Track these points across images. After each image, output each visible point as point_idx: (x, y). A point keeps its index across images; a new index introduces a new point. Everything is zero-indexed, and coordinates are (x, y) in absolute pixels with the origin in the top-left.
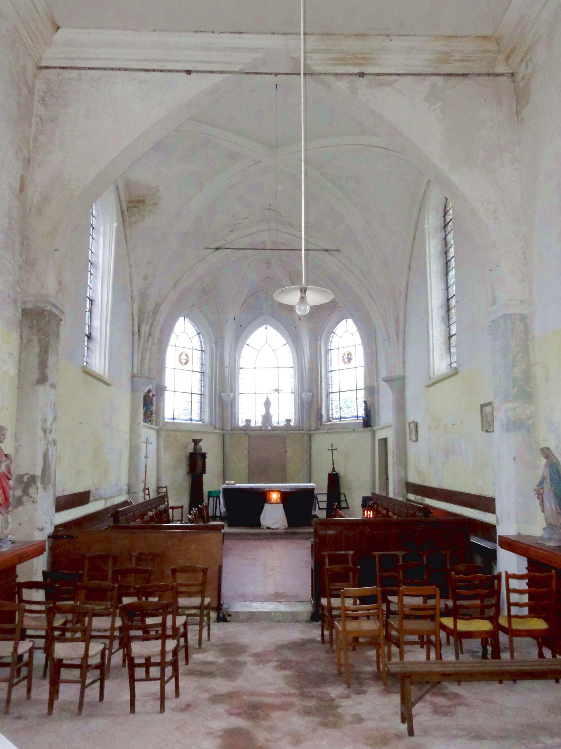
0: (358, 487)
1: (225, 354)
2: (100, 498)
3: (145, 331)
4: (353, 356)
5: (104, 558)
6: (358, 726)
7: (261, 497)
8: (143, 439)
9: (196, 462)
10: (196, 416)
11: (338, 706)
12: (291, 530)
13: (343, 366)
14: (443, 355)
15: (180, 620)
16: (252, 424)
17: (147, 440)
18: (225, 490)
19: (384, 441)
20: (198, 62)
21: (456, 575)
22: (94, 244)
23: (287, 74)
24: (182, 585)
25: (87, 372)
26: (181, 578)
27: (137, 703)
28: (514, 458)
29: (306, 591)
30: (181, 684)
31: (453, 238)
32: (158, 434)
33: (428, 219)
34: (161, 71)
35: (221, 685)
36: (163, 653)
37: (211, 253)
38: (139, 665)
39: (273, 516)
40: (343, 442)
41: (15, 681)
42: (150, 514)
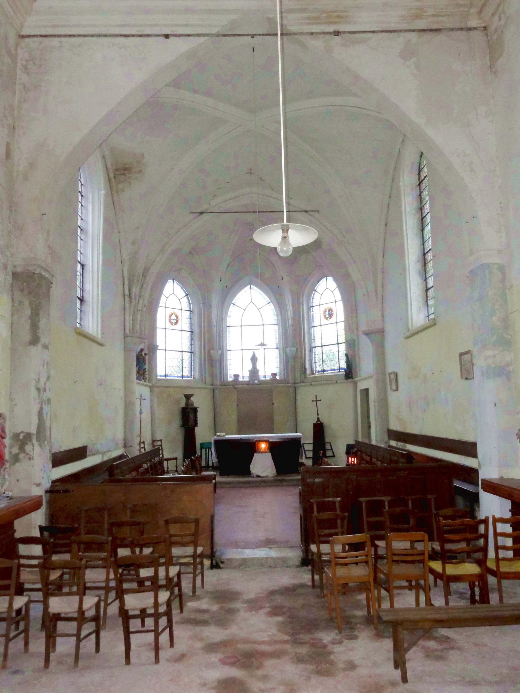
0: (342, 437)
1: (213, 314)
2: (97, 453)
5: (100, 510)
6: (351, 673)
7: (249, 448)
8: (137, 395)
9: (188, 416)
10: (186, 373)
11: (330, 653)
12: (279, 478)
13: (324, 321)
14: (420, 308)
15: (173, 571)
16: (240, 379)
17: (141, 396)
18: (216, 442)
19: (367, 390)
20: (177, 25)
21: (444, 520)
22: (83, 211)
23: (263, 35)
24: (176, 536)
25: (82, 334)
26: (174, 529)
27: (132, 654)
29: (296, 536)
30: (175, 633)
31: (428, 195)
32: (151, 391)
33: (403, 178)
34: (140, 36)
35: (214, 633)
36: (156, 605)
37: (196, 217)
38: (135, 617)
39: (262, 465)
40: (326, 393)
41: (12, 635)
42: (145, 466)
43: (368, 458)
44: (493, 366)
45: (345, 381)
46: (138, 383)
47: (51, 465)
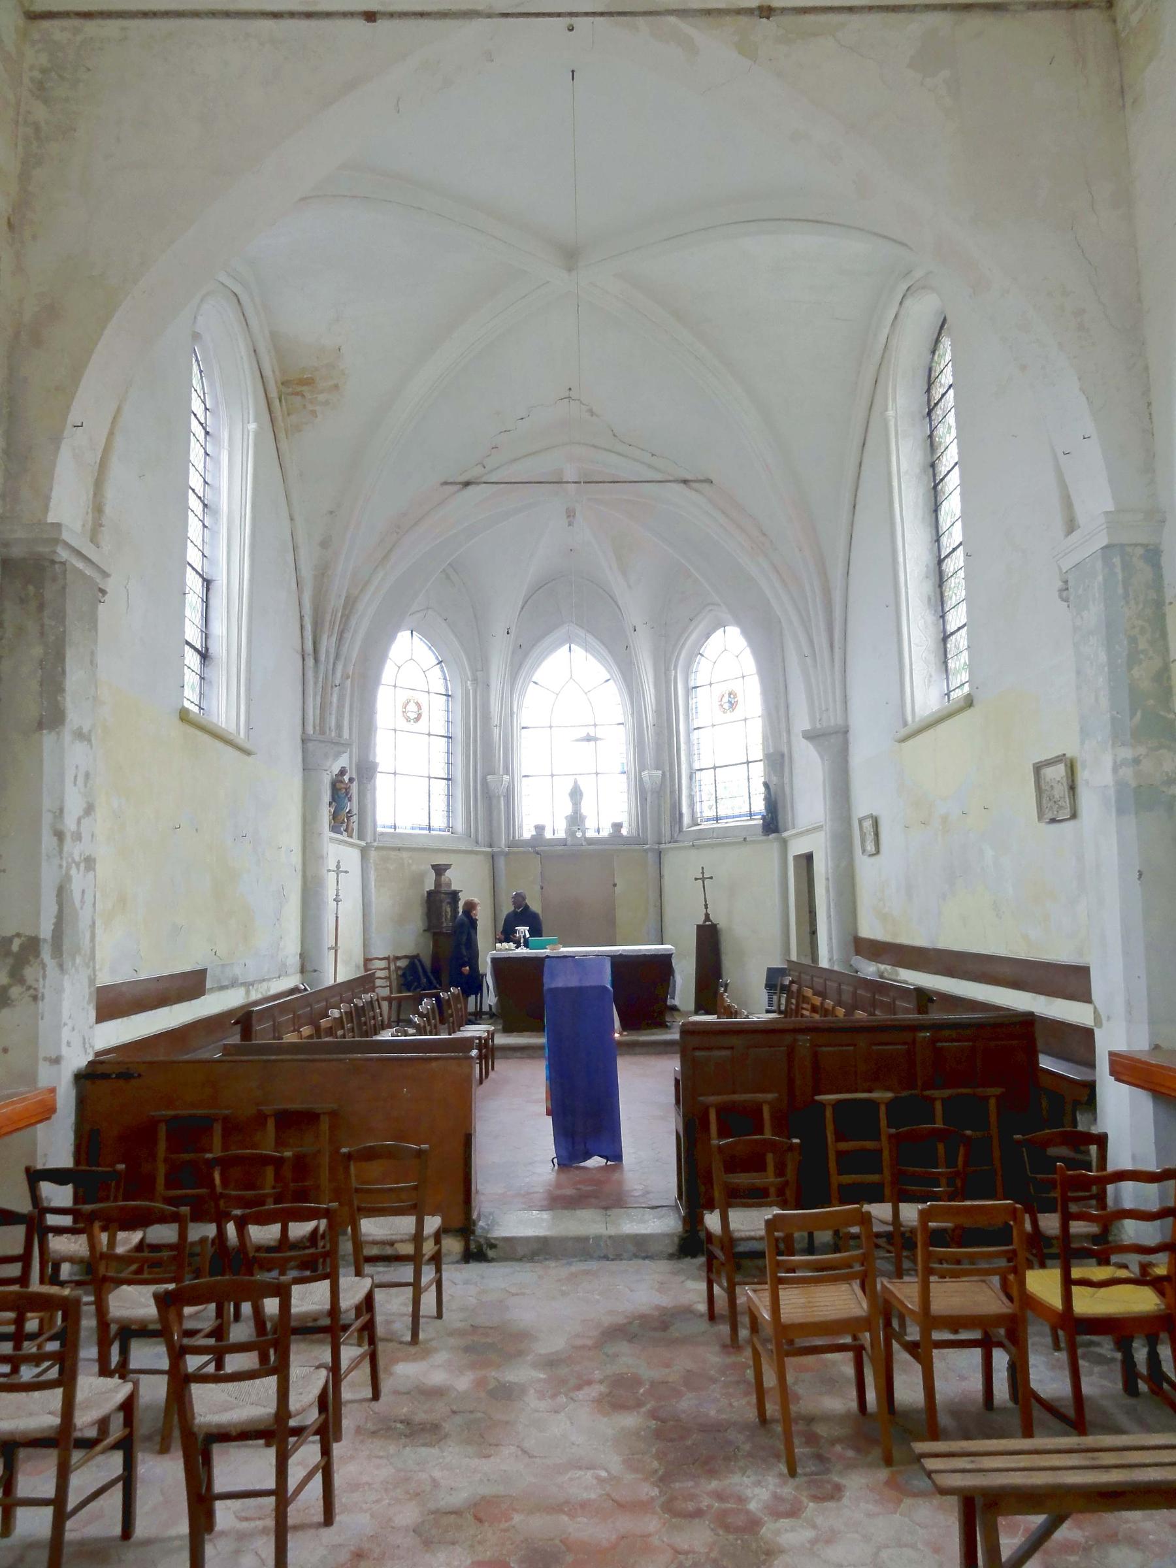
2: (234, 984)
3: (327, 652)
4: (740, 698)
10: (439, 821)
15: (353, 1290)
16: (548, 835)
17: (338, 867)
19: (809, 858)
23: (594, 14)
28: (1140, 875)
33: (894, 400)
42: (335, 1013)
43: (817, 1001)
44: (1133, 784)
45: (764, 838)
46: (332, 839)
47: (93, 1014)
